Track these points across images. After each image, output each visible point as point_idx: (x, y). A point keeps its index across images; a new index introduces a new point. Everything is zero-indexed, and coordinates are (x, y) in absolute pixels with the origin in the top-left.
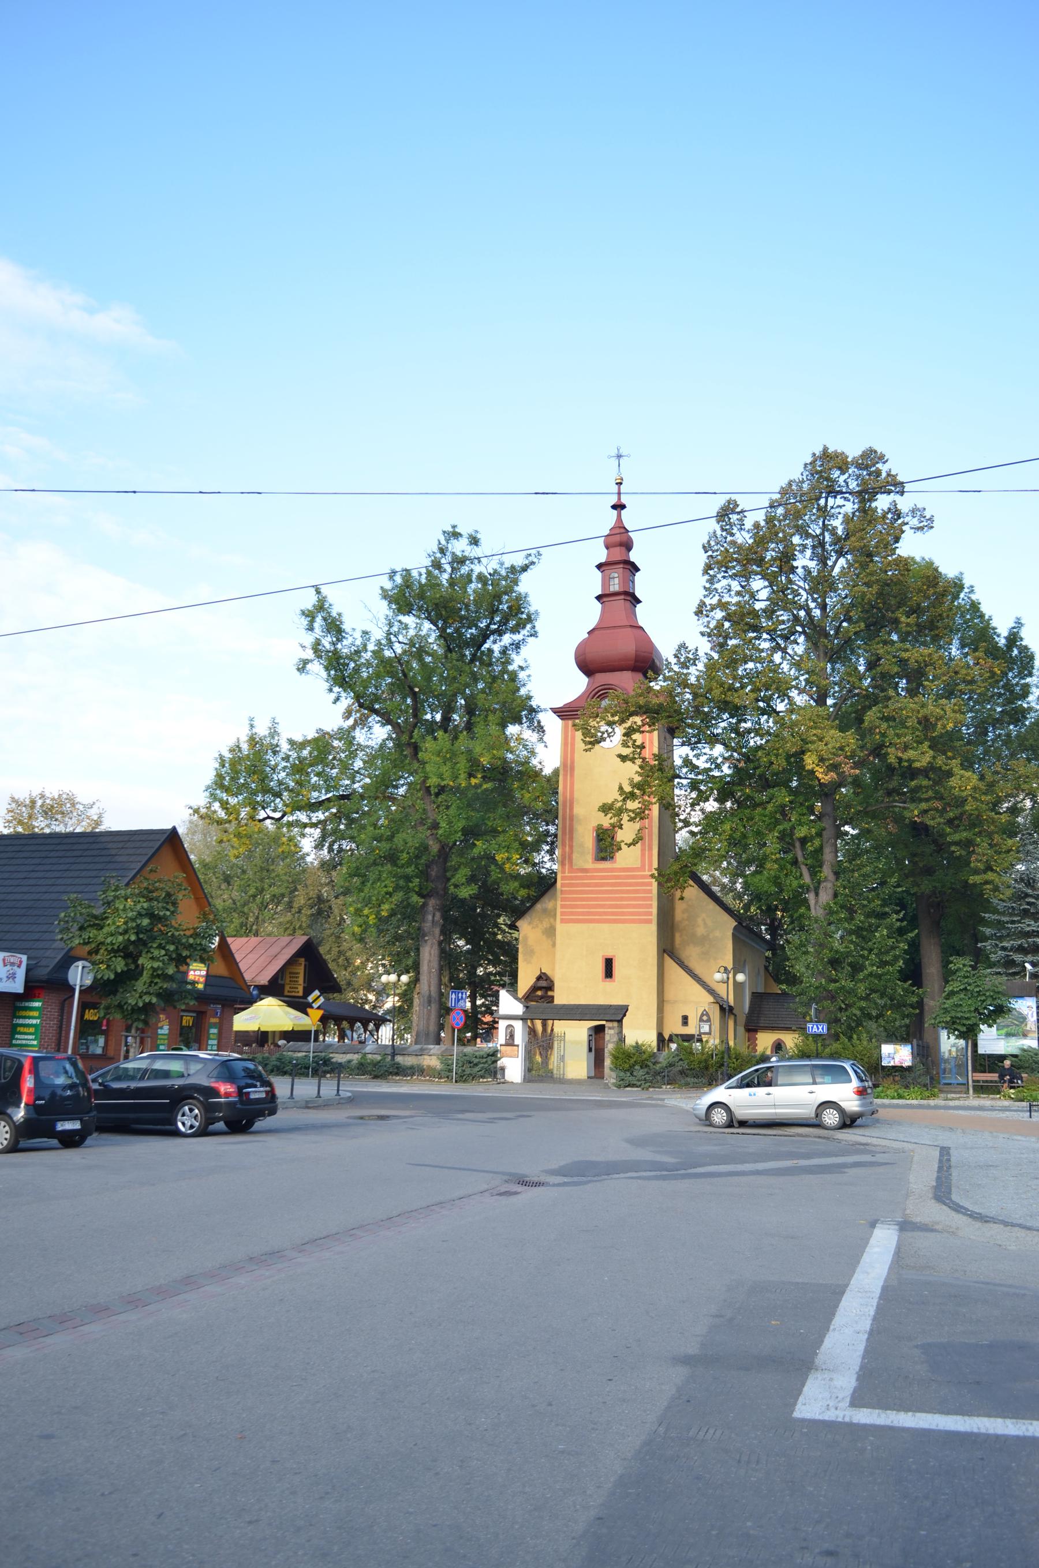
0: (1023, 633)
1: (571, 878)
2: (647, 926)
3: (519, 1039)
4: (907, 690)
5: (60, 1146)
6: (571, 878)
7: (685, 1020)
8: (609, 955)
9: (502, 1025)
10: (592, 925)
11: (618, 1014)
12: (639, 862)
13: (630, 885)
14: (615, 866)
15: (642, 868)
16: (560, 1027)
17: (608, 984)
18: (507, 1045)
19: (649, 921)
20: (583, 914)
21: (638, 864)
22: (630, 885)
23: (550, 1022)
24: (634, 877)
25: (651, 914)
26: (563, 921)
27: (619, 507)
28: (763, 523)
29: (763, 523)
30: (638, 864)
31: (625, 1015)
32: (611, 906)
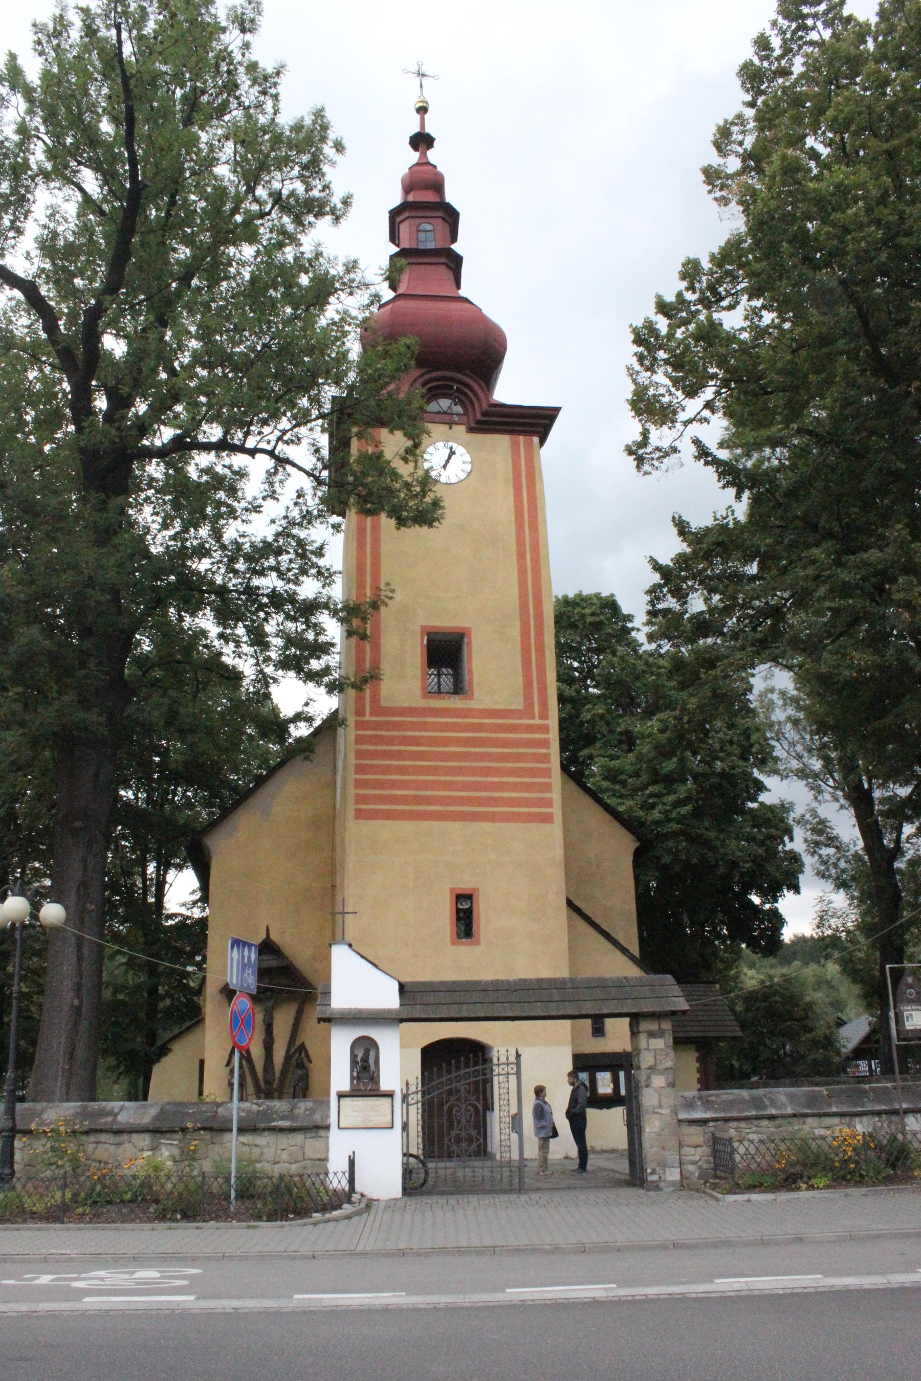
0: (283, 80)
1: (378, 726)
2: (537, 831)
4: (231, 265)
5: (635, 950)
6: (378, 726)
8: (465, 884)
9: (340, 1046)
12: (521, 699)
13: (506, 743)
14: (473, 704)
15: (527, 711)
18: (354, 1093)
19: (547, 819)
20: (404, 800)
21: (518, 704)
22: (506, 743)
24: (512, 729)
25: (549, 803)
26: (360, 815)
27: (421, 141)
28: (706, 265)
29: (706, 265)
30: (518, 704)
32: (466, 786)
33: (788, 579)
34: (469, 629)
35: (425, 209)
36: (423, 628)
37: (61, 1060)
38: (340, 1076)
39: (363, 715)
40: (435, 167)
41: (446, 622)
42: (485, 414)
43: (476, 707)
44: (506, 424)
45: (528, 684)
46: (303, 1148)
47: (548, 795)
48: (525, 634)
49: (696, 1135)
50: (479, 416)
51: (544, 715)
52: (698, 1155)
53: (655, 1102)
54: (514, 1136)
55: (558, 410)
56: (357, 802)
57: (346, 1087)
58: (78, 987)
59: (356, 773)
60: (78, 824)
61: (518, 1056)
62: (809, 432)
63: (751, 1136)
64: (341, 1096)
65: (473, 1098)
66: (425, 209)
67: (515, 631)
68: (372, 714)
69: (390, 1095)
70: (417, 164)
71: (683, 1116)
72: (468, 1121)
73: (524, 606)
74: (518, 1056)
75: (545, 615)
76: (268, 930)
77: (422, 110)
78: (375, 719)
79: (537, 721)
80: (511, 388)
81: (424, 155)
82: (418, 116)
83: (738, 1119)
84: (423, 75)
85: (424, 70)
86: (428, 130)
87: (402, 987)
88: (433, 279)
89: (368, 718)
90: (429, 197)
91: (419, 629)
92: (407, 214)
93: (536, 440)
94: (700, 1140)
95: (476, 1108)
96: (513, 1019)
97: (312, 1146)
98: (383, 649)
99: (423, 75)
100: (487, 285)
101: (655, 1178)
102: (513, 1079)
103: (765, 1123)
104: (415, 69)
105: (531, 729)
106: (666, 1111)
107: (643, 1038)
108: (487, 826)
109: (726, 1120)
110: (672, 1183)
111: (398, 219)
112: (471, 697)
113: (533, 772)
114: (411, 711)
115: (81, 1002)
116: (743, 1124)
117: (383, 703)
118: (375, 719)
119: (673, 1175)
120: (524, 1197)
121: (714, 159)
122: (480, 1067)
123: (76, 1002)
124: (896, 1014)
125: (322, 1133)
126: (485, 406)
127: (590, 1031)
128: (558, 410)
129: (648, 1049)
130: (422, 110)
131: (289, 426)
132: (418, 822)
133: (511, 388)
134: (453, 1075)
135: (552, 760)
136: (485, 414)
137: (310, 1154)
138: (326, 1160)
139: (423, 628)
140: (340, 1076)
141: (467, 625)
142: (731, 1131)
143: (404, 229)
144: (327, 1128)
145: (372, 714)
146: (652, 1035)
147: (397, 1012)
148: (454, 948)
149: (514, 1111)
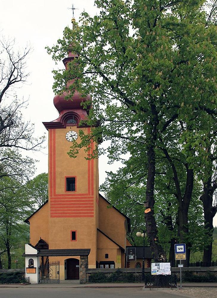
1: (55, 198)
3: (36, 264)
7: (107, 256)
8: (74, 230)
10: (66, 218)
11: (85, 253)
16: (52, 259)
17: (74, 242)
19: (92, 216)
23: (45, 258)
31: (89, 253)
32: (74, 210)
34: (76, 176)
36: (65, 177)
38: (27, 265)
39: (52, 196)
41: (70, 175)
43: (77, 193)
45: (89, 188)
47: (93, 211)
48: (89, 177)
51: (93, 194)
54: (58, 275)
56: (93, 203)
57: (28, 267)
59: (51, 208)
61: (59, 262)
62: (122, 137)
64: (27, 268)
67: (87, 176)
68: (54, 196)
69: (36, 268)
73: (89, 170)
74: (59, 262)
75: (94, 172)
76: (41, 238)
78: (54, 197)
79: (91, 196)
84: (74, 9)
85: (74, 7)
89: (53, 197)
91: (64, 177)
98: (56, 182)
99: (74, 9)
102: (58, 266)
105: (89, 198)
108: (79, 218)
112: (76, 191)
113: (89, 207)
114: (63, 195)
117: (56, 194)
118: (54, 197)
121: (53, 90)
124: (128, 257)
127: (109, 255)
131: (109, 93)
132: (64, 218)
135: (94, 204)
139: (65, 177)
140: (27, 265)
141: (75, 175)
145: (54, 196)
148: (71, 242)
149: (58, 271)
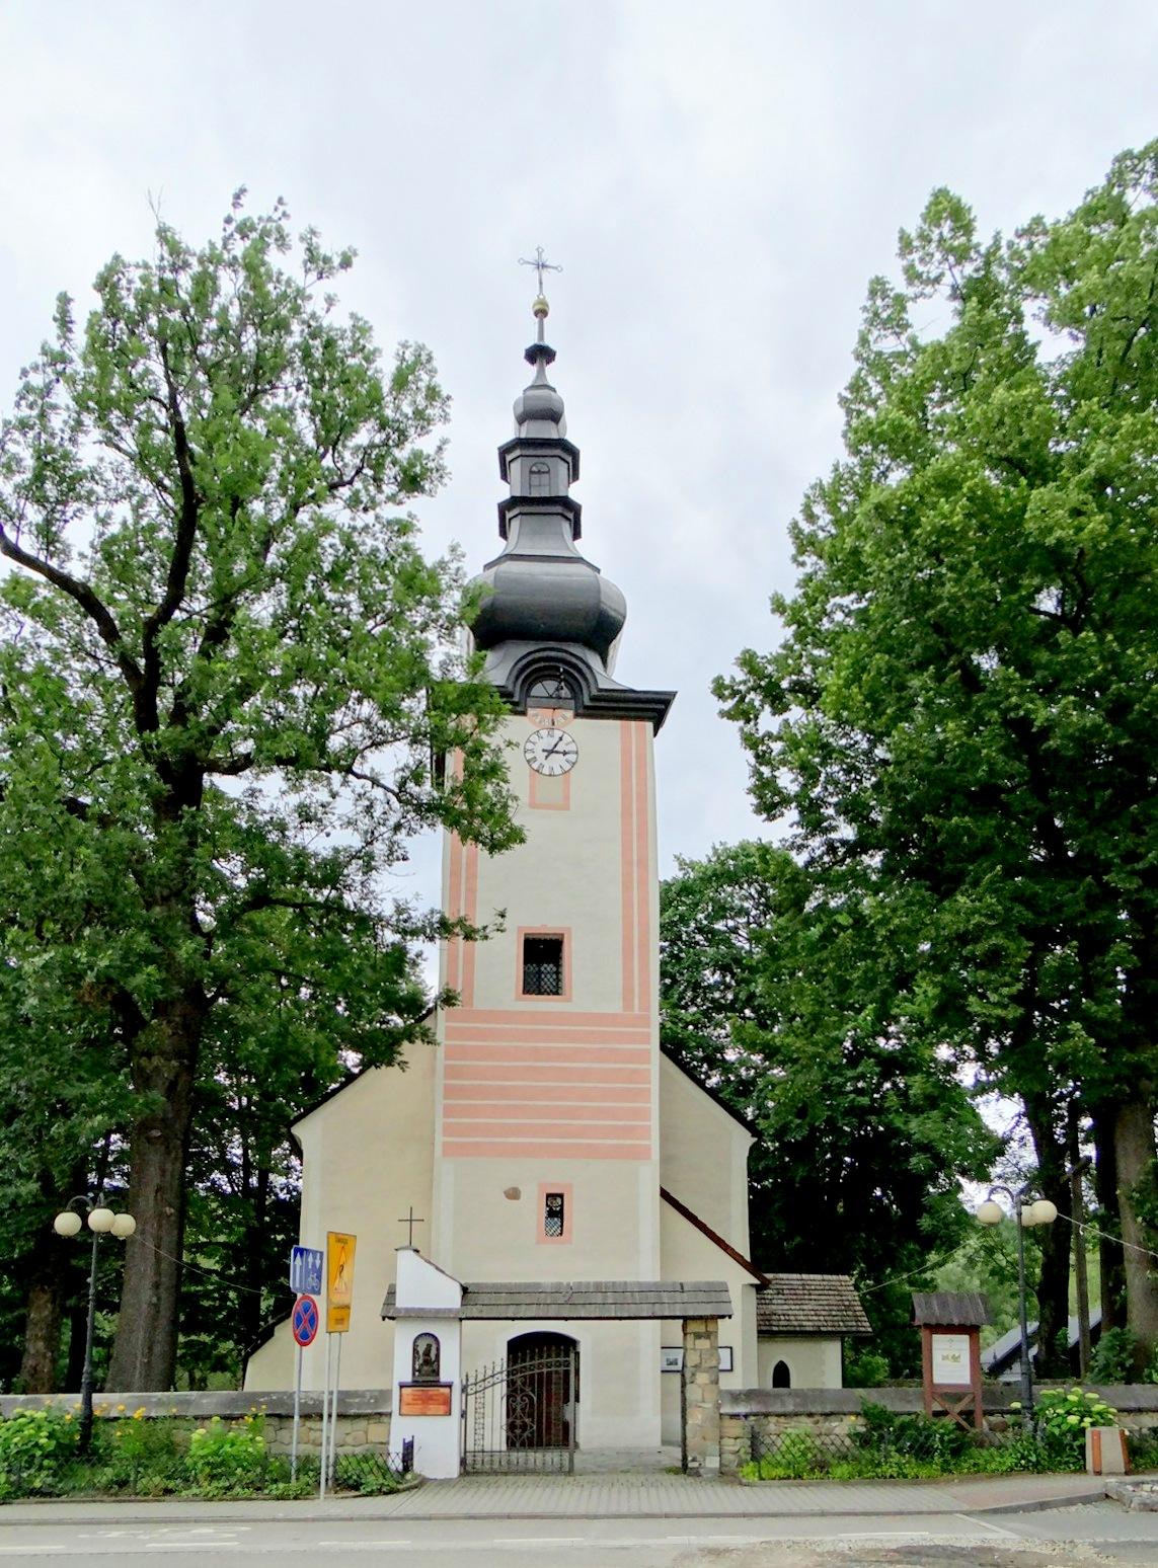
5: (744, 1250)
33: (1068, 1407)
35: (541, 447)
37: (139, 1354)
40: (554, 390)
42: (593, 699)
44: (614, 709)
46: (366, 1433)
49: (735, 1428)
50: (587, 702)
52: (736, 1444)
53: (699, 1398)
55: (674, 694)
58: (157, 1286)
60: (156, 1133)
63: (789, 1431)
65: (528, 1389)
66: (541, 447)
70: (533, 387)
71: (727, 1409)
72: (523, 1409)
77: (541, 313)
80: (627, 667)
81: (541, 373)
82: (537, 320)
83: (779, 1415)
84: (544, 266)
86: (548, 342)
87: (465, 1290)
88: (551, 538)
90: (548, 431)
92: (517, 452)
93: (650, 725)
94: (738, 1431)
95: (531, 1399)
96: (566, 1319)
97: (375, 1431)
99: (544, 266)
100: (608, 551)
101: (696, 1465)
103: (804, 1419)
104: (533, 256)
106: (708, 1405)
107: (690, 1338)
109: (766, 1415)
110: (711, 1470)
111: (509, 458)
115: (159, 1299)
116: (782, 1419)
119: (713, 1463)
120: (571, 1479)
122: (562, 1359)
123: (154, 1300)
125: (385, 1419)
126: (594, 692)
128: (674, 694)
129: (694, 1349)
130: (541, 313)
133: (627, 667)
134: (536, 1362)
136: (593, 699)
137: (373, 1438)
138: (387, 1443)
142: (772, 1425)
143: (515, 469)
144: (389, 1415)
146: (698, 1336)
147: (458, 1311)
